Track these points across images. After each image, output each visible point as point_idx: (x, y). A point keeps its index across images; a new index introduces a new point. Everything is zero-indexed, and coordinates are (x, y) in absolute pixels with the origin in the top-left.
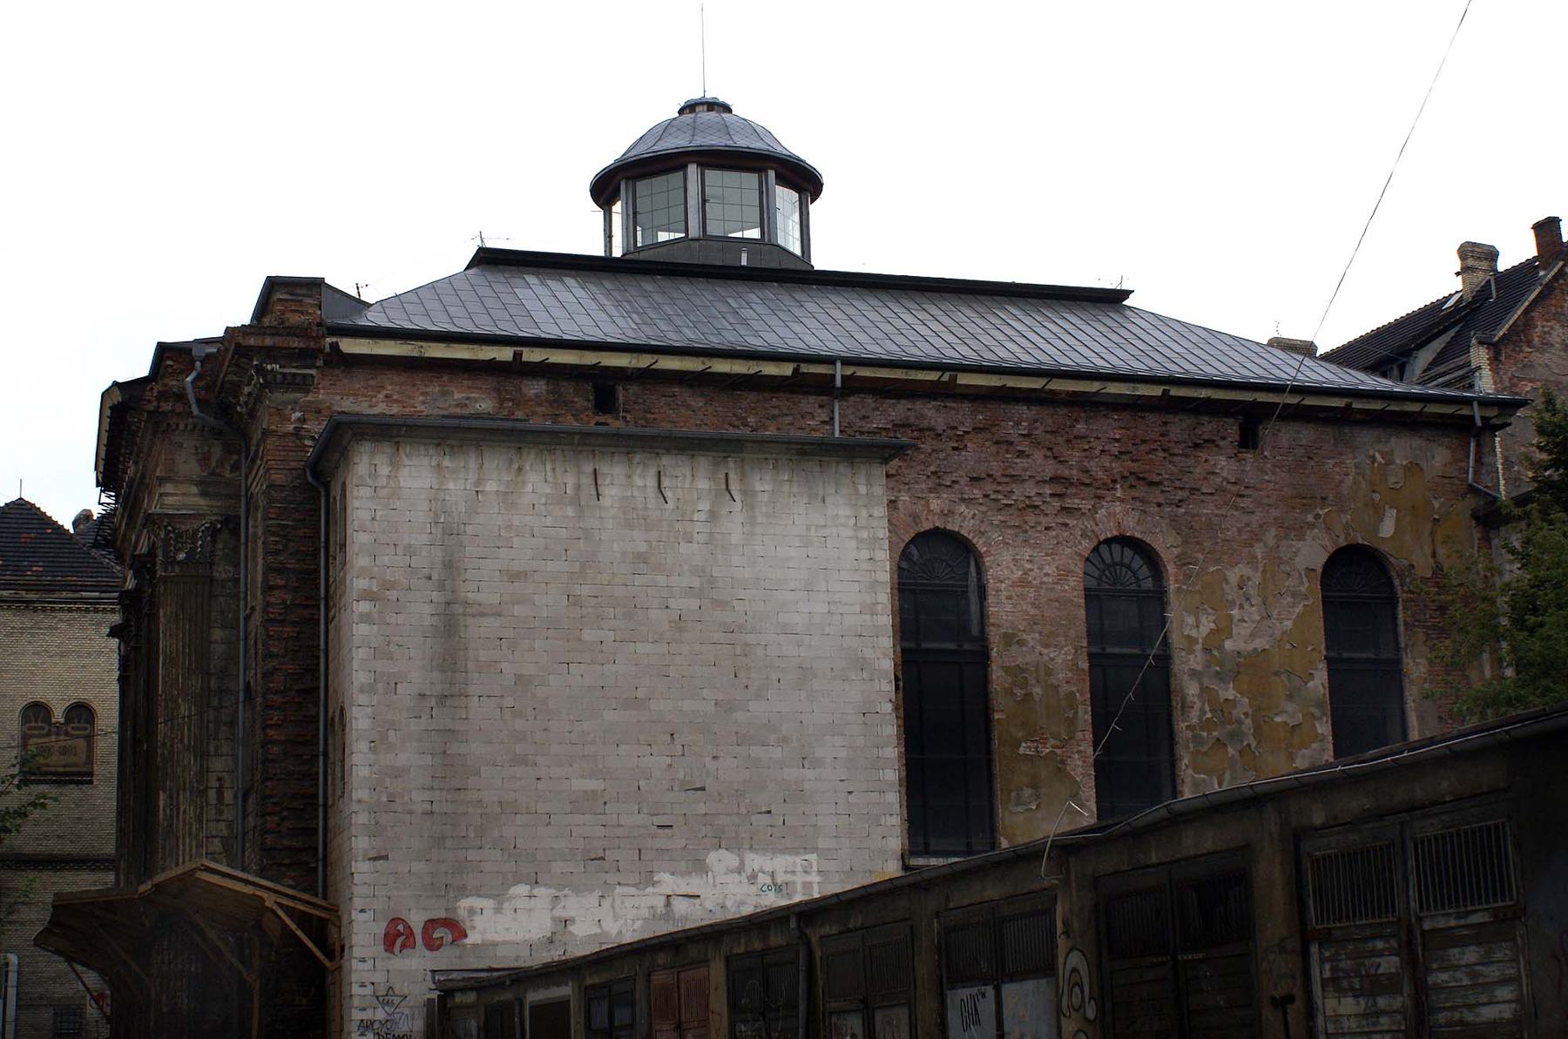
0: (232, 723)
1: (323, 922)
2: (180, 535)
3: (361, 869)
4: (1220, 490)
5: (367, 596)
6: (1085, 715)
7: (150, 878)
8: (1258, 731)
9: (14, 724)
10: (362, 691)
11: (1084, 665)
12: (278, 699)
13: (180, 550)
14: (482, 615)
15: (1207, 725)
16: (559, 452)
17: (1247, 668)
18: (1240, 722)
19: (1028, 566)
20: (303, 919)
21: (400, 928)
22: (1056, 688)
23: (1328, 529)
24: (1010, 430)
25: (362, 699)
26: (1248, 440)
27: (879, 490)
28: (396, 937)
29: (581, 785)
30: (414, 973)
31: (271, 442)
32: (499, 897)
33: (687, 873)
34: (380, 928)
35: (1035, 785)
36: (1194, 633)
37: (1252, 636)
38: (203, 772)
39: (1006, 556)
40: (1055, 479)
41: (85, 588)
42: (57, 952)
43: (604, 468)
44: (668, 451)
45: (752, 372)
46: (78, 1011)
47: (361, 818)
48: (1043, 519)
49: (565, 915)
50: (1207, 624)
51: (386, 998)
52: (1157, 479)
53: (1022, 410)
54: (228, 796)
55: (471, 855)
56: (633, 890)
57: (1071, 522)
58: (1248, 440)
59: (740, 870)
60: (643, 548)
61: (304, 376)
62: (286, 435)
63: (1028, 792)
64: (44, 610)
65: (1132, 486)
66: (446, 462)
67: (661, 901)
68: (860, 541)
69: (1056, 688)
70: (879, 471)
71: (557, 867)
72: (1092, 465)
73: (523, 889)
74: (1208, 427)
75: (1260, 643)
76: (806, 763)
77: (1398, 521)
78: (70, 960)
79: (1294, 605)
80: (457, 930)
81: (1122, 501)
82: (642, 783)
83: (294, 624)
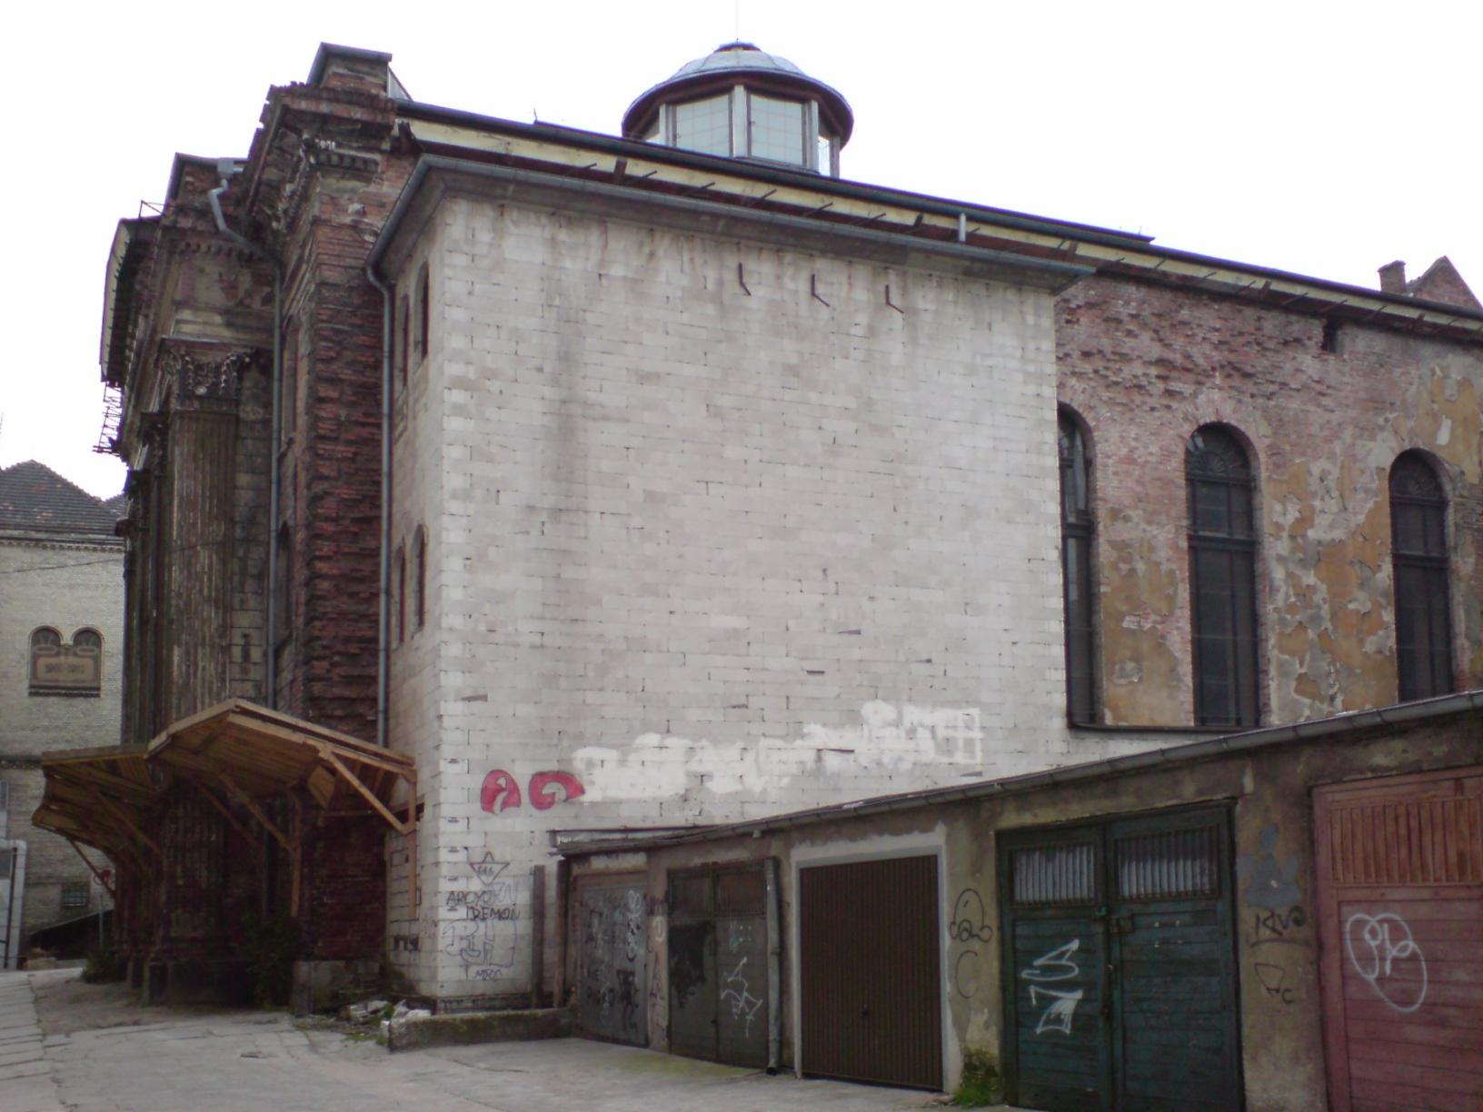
0: (262, 576)
1: (390, 778)
2: (199, 367)
3: (453, 710)
4: (1306, 387)
5: (460, 383)
6: (1184, 594)
7: (164, 726)
8: (1334, 616)
9: (24, 644)
10: (454, 496)
11: (1184, 544)
12: (330, 528)
13: (199, 384)
14: (605, 418)
15: (1291, 609)
16: (697, 241)
17: (1325, 557)
18: (1319, 607)
19: (1134, 444)
20: (365, 773)
21: (502, 782)
22: (1158, 564)
23: (1396, 432)
24: (1121, 309)
25: (455, 506)
26: (1329, 345)
27: (1047, 322)
28: (496, 793)
29: (721, 622)
30: (524, 840)
31: (323, 233)
32: (624, 747)
33: (840, 726)
34: (477, 782)
35: (1137, 658)
36: (1281, 520)
37: (1332, 526)
38: (225, 628)
39: (1114, 432)
40: (1160, 362)
41: (92, 531)
42: (60, 831)
43: (751, 264)
44: (823, 253)
45: (872, 216)
46: (84, 887)
47: (453, 650)
48: (1147, 399)
49: (701, 769)
50: (1293, 514)
51: (482, 865)
52: (1249, 369)
53: (1132, 291)
54: (256, 654)
55: (591, 697)
56: (779, 743)
57: (1174, 405)
58: (1329, 345)
59: (897, 724)
60: (794, 360)
61: (366, 161)
62: (342, 226)
63: (1130, 666)
64: (53, 548)
65: (1229, 376)
66: (563, 235)
67: (809, 757)
68: (1028, 375)
69: (1158, 564)
70: (1048, 302)
71: (693, 715)
72: (1194, 351)
73: (652, 739)
74: (1297, 326)
75: (1338, 534)
76: (969, 609)
77: (1453, 430)
78: (73, 838)
79: (1366, 501)
80: (572, 784)
81: (1220, 389)
82: (791, 623)
83: (349, 443)
